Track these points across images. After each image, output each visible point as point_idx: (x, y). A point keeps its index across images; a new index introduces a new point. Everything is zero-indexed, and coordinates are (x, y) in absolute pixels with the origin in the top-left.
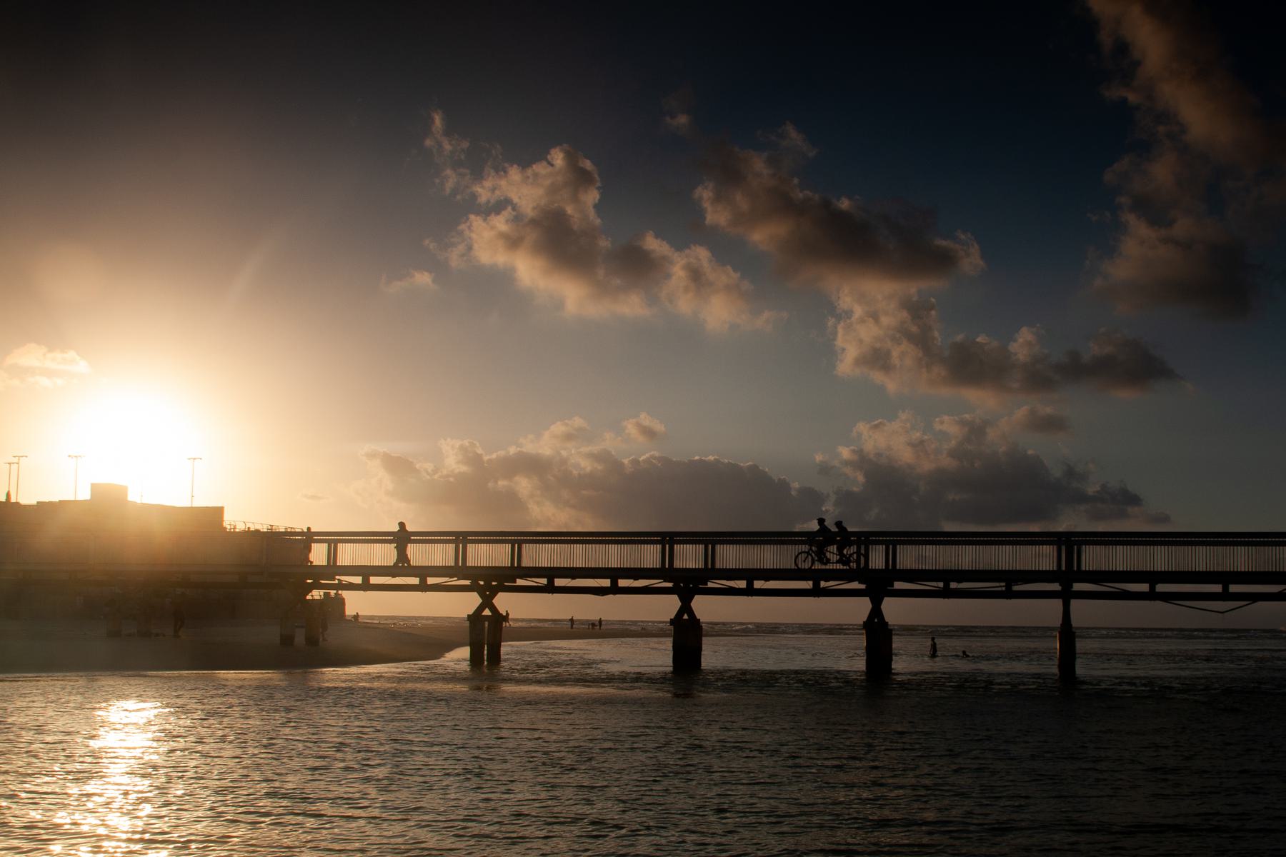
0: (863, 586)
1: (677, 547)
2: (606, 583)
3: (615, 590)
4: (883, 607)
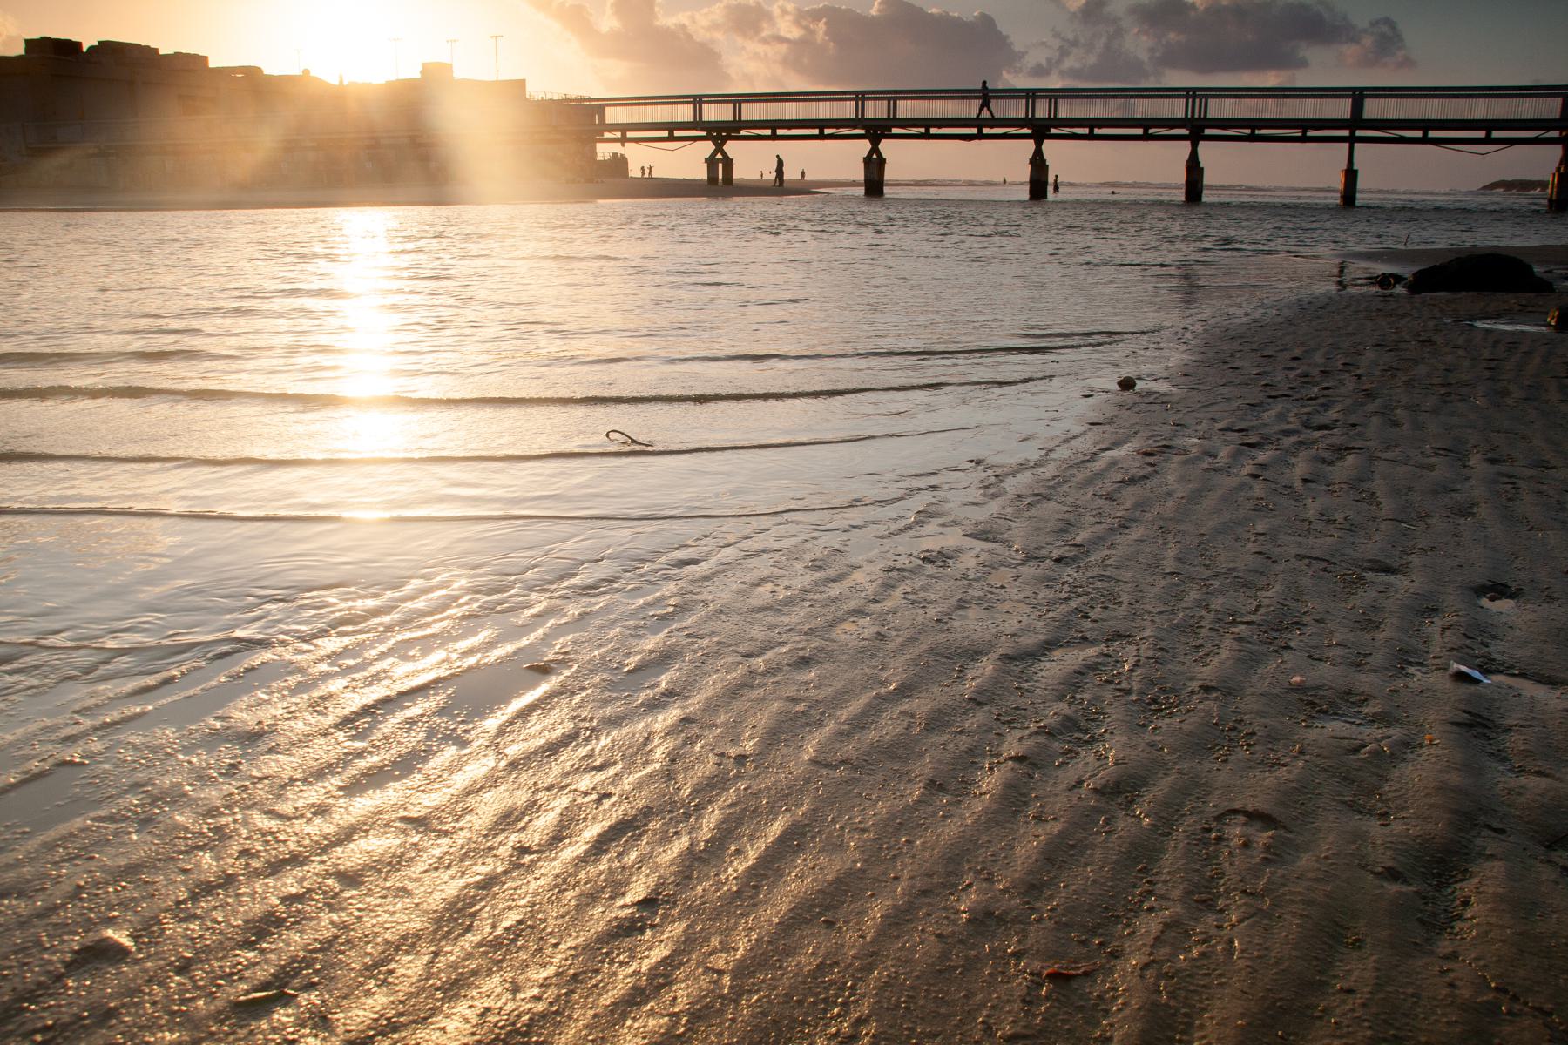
0: (1029, 131)
2: (768, 132)
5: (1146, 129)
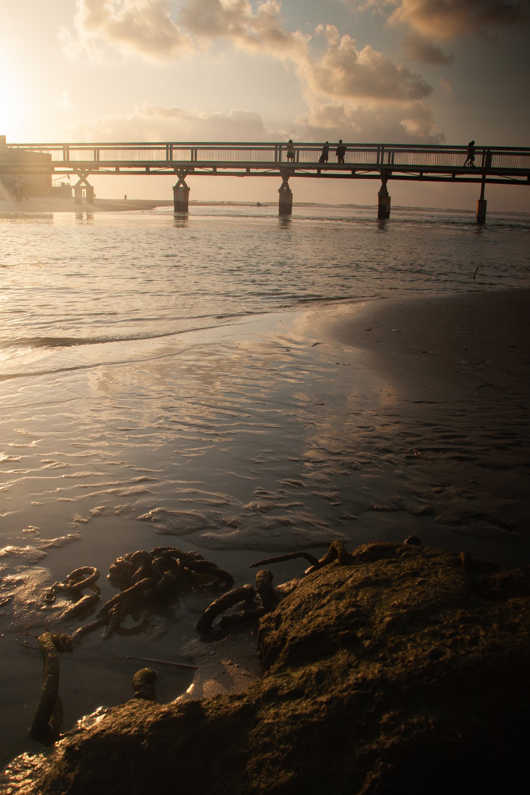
1: (62, 151)
3: (248, 174)
4: (289, 182)
5: (354, 171)
